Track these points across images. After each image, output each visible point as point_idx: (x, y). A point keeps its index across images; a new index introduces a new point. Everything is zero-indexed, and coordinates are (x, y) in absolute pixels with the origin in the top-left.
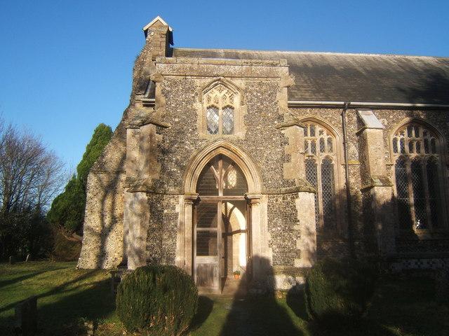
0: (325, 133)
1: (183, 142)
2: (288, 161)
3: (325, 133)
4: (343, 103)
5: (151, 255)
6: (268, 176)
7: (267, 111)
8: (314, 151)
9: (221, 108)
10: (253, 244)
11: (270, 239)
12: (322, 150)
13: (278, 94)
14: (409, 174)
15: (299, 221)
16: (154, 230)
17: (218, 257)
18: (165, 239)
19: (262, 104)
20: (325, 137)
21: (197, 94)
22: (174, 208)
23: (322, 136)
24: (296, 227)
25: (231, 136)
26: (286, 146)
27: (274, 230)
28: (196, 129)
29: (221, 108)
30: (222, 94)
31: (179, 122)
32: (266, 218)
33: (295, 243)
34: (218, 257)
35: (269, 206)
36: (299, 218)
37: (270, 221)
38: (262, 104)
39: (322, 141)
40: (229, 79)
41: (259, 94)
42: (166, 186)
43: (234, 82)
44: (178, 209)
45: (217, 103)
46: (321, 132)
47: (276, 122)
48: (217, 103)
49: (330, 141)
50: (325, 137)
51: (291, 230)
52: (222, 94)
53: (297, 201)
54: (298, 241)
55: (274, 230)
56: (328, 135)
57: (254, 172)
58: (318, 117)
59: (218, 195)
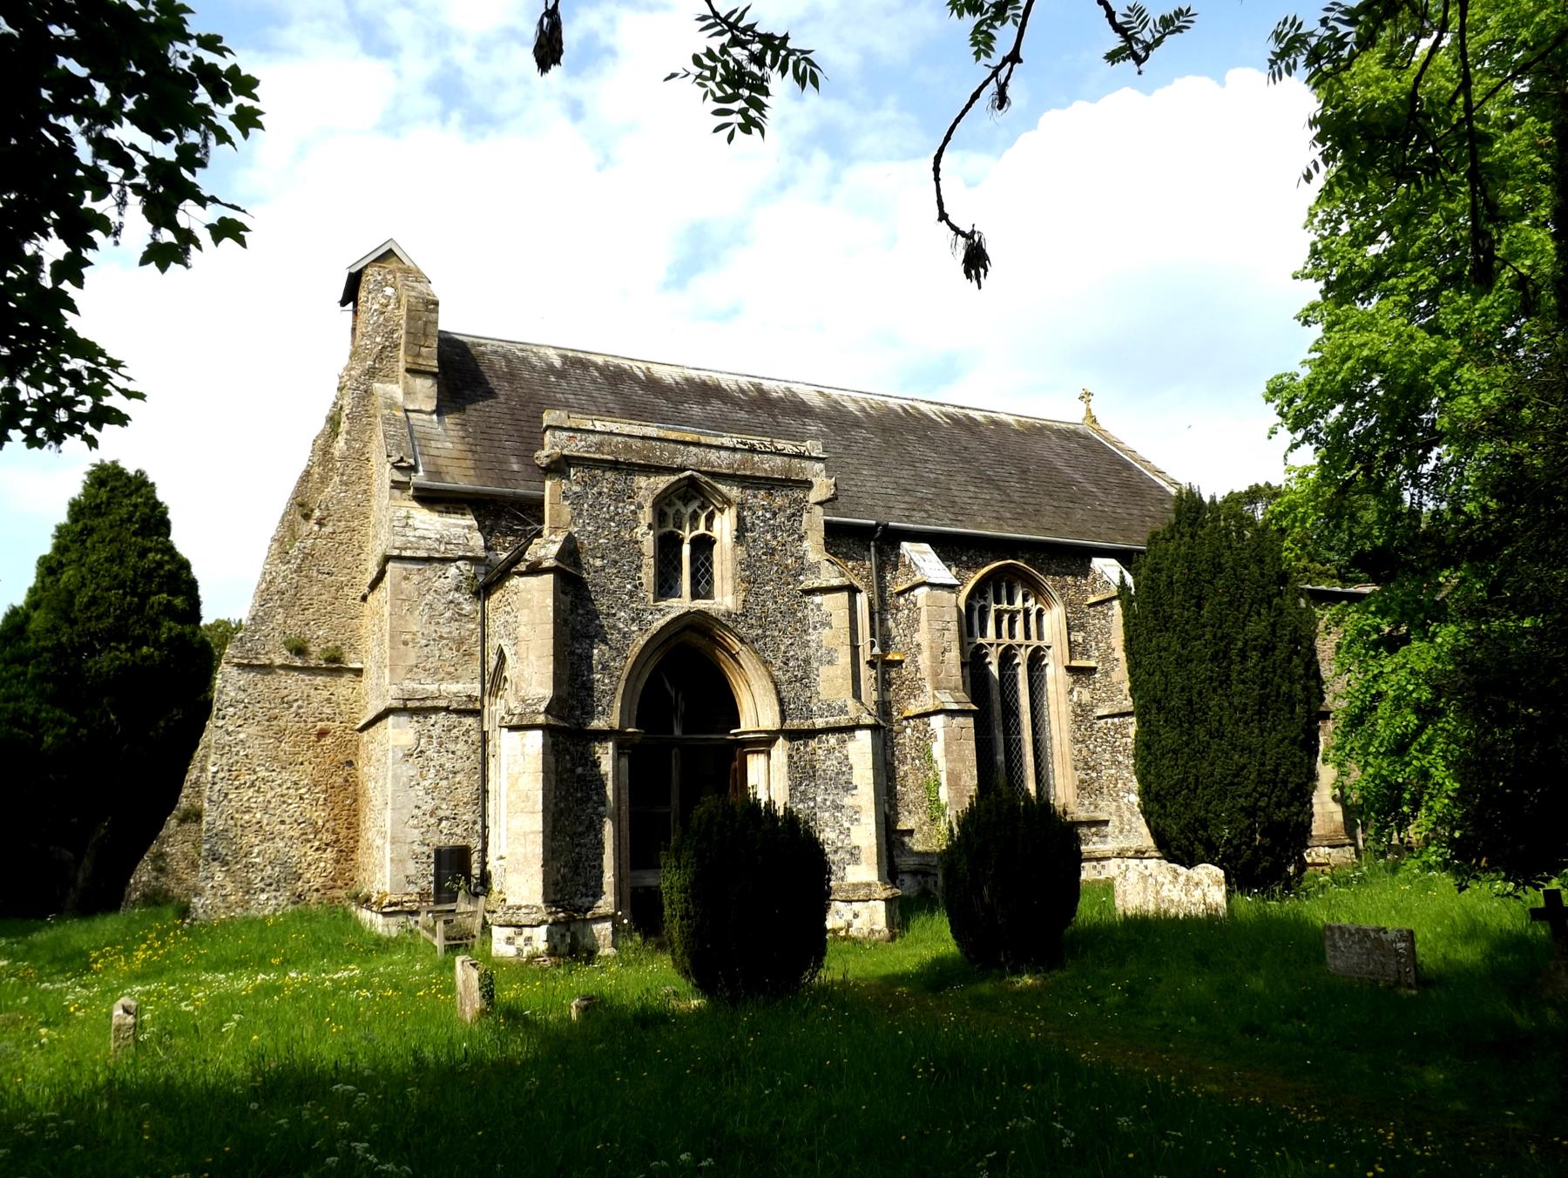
2: (830, 662)
13: (805, 516)
19: (775, 537)
30: (690, 510)
31: (603, 568)
35: (790, 757)
38: (775, 537)
51: (839, 808)
59: (672, 732)
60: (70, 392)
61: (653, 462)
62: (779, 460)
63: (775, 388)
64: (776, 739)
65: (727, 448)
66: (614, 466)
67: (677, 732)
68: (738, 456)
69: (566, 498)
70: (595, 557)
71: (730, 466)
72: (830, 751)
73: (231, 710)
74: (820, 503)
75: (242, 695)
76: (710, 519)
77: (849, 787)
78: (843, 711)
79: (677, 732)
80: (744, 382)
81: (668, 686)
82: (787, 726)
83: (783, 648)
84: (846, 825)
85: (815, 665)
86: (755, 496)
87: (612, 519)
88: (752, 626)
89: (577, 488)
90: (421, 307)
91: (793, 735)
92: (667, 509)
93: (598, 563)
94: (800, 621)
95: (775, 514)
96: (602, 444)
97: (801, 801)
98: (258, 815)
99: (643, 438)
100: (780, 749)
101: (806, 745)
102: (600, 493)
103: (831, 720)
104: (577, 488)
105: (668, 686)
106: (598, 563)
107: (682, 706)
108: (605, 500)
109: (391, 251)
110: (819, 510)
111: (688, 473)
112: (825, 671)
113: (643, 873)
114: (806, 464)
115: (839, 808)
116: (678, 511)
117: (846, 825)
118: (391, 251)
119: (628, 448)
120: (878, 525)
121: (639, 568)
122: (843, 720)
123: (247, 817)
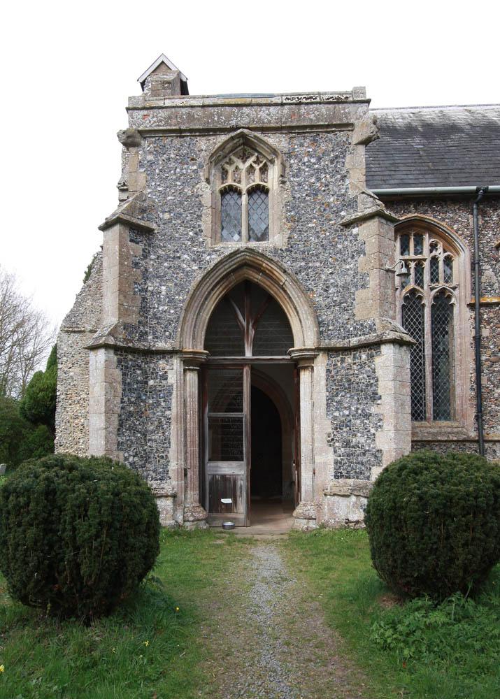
0: (440, 249)
1: (179, 258)
2: (363, 286)
3: (440, 249)
4: (474, 188)
5: (126, 459)
6: (327, 316)
7: (327, 192)
8: (419, 281)
9: (244, 191)
10: (302, 441)
11: (330, 430)
12: (434, 278)
13: (348, 157)
14: (368, 501)
15: (380, 398)
16: (130, 414)
17: (244, 463)
18: (153, 432)
19: (319, 179)
20: (440, 253)
21: (201, 166)
22: (165, 377)
23: (434, 253)
24: (373, 410)
25: (263, 244)
26: (361, 259)
27: (336, 414)
28: (201, 231)
29: (244, 191)
30: (247, 164)
31: (170, 220)
32: (324, 394)
33: (372, 437)
34: (244, 463)
35: (328, 371)
36: (380, 392)
37: (330, 400)
38: (319, 179)
39: (434, 261)
40: (258, 134)
41: (313, 160)
42: (150, 337)
43: (265, 139)
44: (172, 379)
45: (239, 182)
46: (433, 247)
47: (343, 213)
48: (239, 182)
49: (448, 261)
50: (440, 253)
51: (367, 416)
52: (247, 164)
53: (378, 360)
54: (377, 434)
55: (336, 414)
56: (445, 251)
57: (304, 310)
58: (429, 217)
59: (244, 355)
60: (359, 277)
61: (211, 126)
62: (323, 108)
63: (430, 116)
64: (315, 357)
65: (276, 105)
66: (180, 133)
67: (248, 354)
68: (286, 109)
69: (141, 166)
70: (164, 212)
71: (279, 119)
72: (362, 365)
73: (65, 358)
74: (361, 143)
75: (71, 350)
76: (264, 170)
77: (375, 397)
78: (372, 329)
79: (248, 354)
80: (406, 113)
81: (241, 318)
82: (325, 343)
83: (323, 277)
84: (373, 431)
85: (353, 290)
86: (302, 145)
87: (178, 179)
88: (296, 260)
89: (150, 157)
90: (160, 87)
91: (331, 351)
92: (227, 167)
93: (167, 216)
94: (340, 252)
95: (319, 159)
96: (170, 118)
97: (337, 409)
98: (82, 421)
99: (203, 106)
100: (321, 364)
101: (343, 361)
102: (169, 159)
103: (363, 338)
104: (150, 157)
105: (241, 318)
106: (167, 216)
107: (252, 333)
108: (172, 165)
109: (163, 62)
110: (362, 149)
111: (239, 131)
112: (360, 294)
113: (220, 464)
114: (350, 108)
115: (367, 416)
116: (237, 168)
117: (373, 431)
118: (163, 62)
119: (191, 117)
120: (478, 190)
121: (199, 217)
122: (372, 337)
123: (76, 421)
